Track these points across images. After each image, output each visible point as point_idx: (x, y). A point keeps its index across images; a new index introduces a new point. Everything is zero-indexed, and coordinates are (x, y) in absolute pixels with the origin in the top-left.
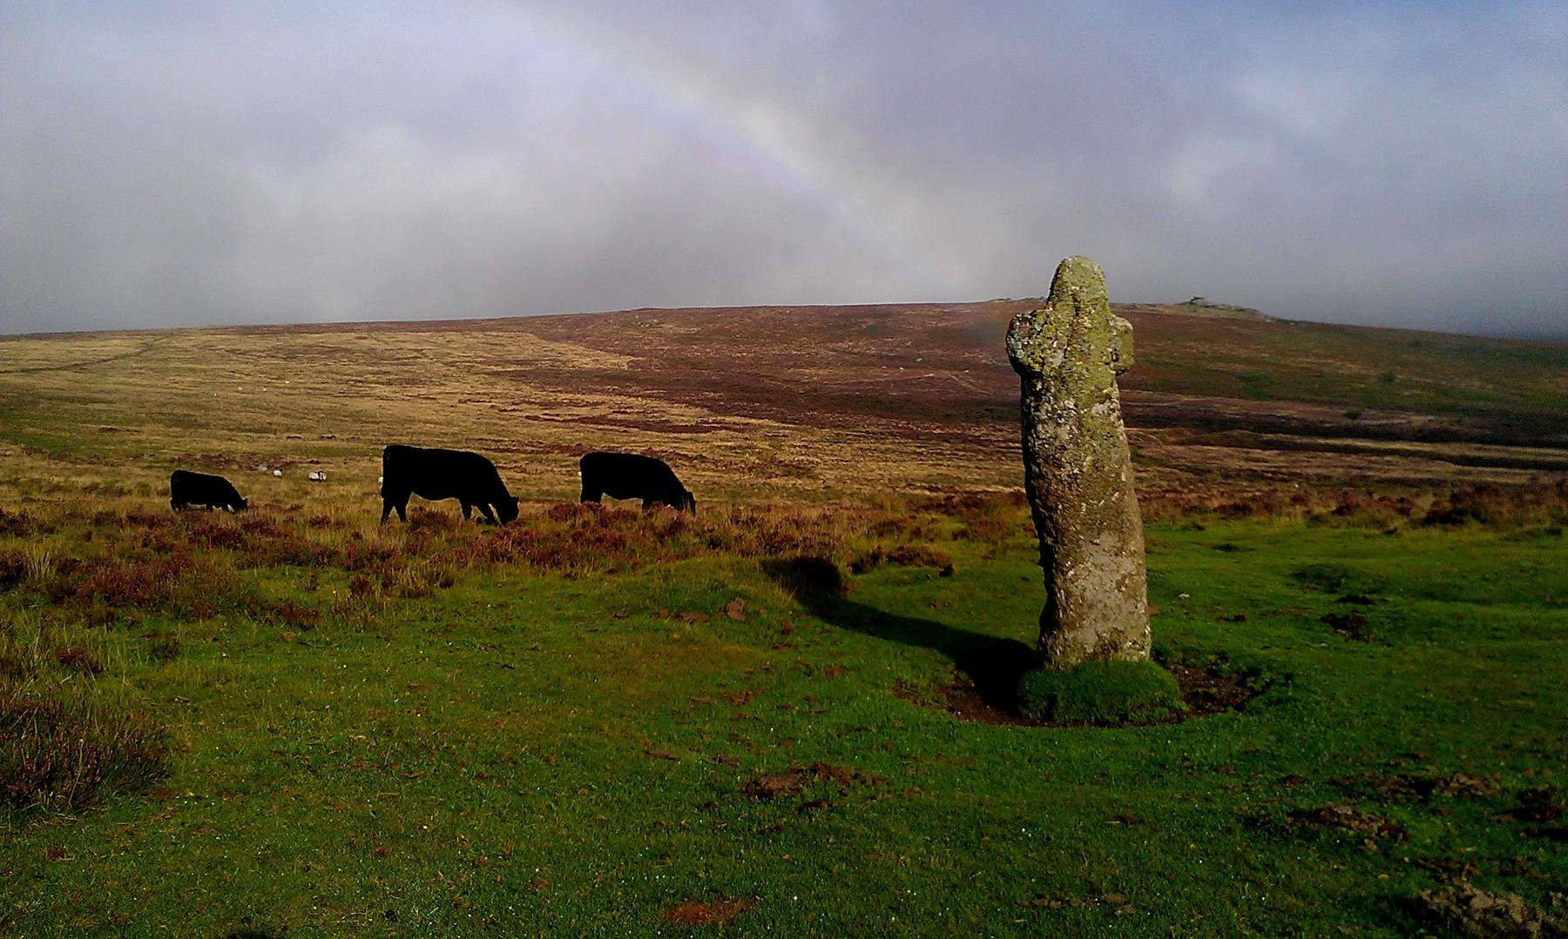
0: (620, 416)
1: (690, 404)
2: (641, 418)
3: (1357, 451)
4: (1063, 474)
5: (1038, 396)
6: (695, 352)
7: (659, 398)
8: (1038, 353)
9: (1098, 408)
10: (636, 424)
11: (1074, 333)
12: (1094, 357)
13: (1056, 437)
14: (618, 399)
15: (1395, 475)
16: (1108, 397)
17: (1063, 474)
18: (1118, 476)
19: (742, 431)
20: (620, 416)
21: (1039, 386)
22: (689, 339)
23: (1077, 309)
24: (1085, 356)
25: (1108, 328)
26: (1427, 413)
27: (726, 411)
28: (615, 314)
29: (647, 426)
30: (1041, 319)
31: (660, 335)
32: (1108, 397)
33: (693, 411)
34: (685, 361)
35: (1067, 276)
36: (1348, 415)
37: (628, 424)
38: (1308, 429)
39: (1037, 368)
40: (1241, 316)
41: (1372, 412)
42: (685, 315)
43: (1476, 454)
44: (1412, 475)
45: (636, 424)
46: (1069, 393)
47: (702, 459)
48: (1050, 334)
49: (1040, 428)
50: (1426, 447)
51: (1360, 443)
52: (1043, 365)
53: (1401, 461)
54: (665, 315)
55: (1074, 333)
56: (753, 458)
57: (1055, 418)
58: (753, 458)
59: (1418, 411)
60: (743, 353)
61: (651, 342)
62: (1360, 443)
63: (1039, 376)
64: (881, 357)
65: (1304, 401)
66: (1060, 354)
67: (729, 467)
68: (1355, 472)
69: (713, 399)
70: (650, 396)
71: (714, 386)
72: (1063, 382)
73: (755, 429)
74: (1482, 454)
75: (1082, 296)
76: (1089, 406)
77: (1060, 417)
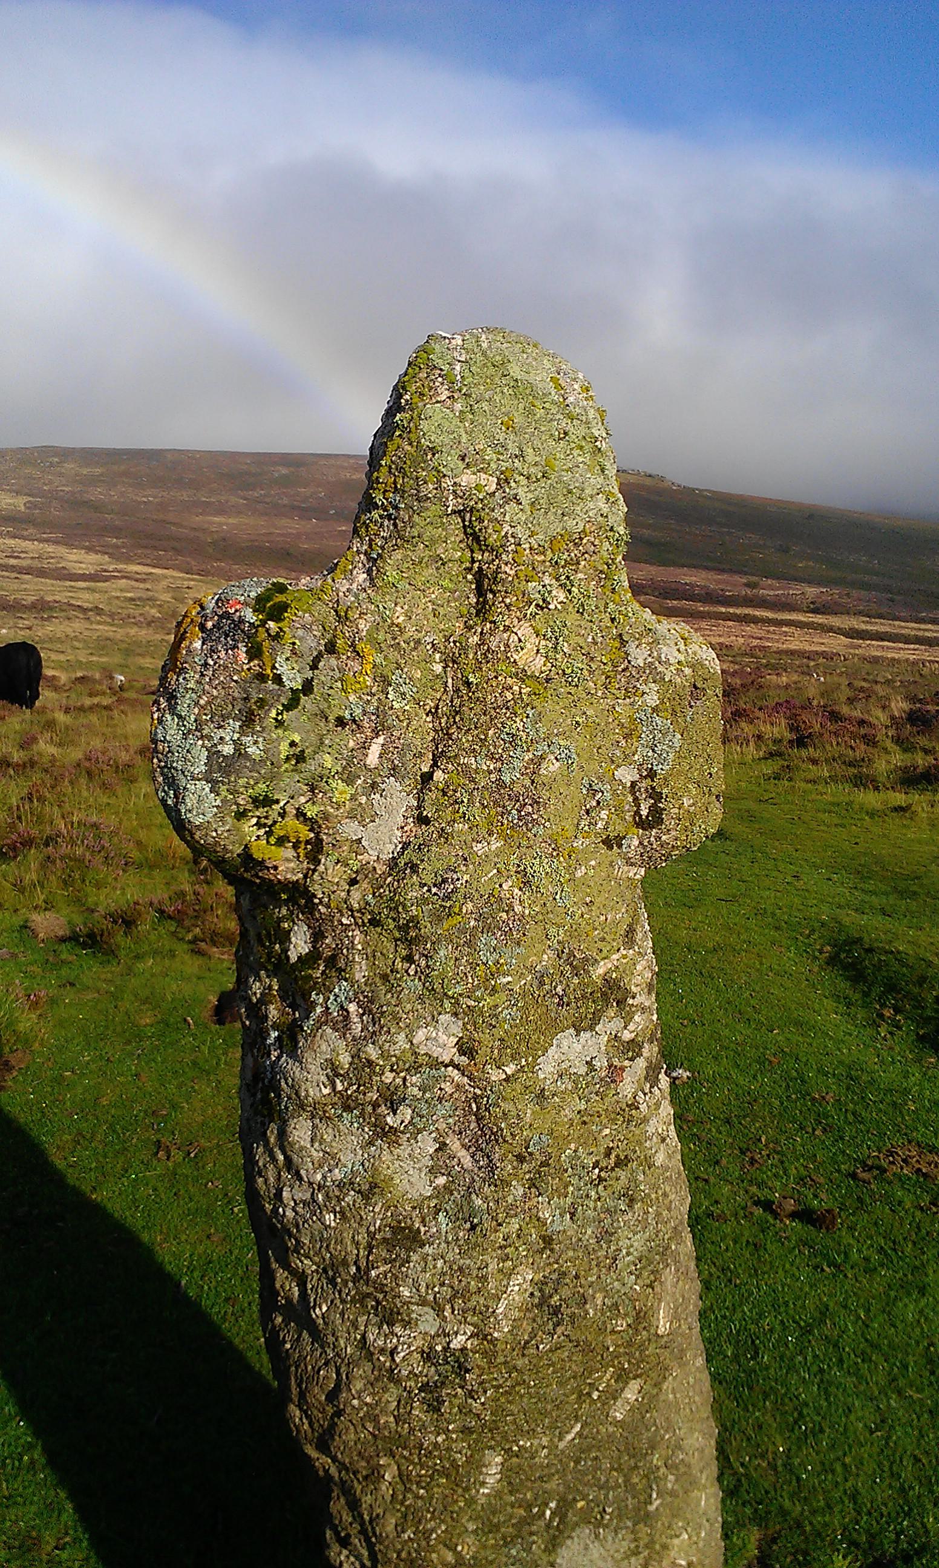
0: (12, 562)
1: (89, 549)
2: (36, 564)
3: (755, 620)
4: (407, 1345)
5: (297, 990)
6: (97, 494)
7: (56, 542)
8: (289, 791)
9: (572, 1050)
10: (28, 571)
11: (465, 706)
12: (558, 814)
13: (371, 1191)
14: (12, 542)
15: (792, 647)
16: (614, 993)
17: (407, 1345)
18: (642, 1318)
19: (144, 581)
20: (12, 562)
21: (300, 944)
22: (93, 481)
23: (484, 584)
24: (516, 808)
25: (622, 676)
26: (819, 584)
27: (128, 560)
28: (12, 450)
29: (41, 573)
30: (303, 630)
31: (61, 475)
32: (614, 993)
33: (93, 557)
34: (86, 503)
35: (437, 420)
36: (747, 585)
37: (21, 570)
38: (709, 597)
39: (286, 865)
40: (648, 482)
41: (769, 582)
42: (90, 456)
43: (863, 627)
44: (807, 648)
45: (28, 571)
46: (435, 994)
47: (98, 611)
48: (352, 704)
49: (300, 1131)
50: (819, 619)
51: (758, 613)
52: (315, 850)
53: (798, 632)
54: (66, 454)
55: (465, 706)
56: (153, 611)
57: (371, 1102)
58: (153, 611)
59: (810, 582)
60: (149, 496)
61: (51, 482)
62: (758, 613)
63: (299, 896)
64: (293, 508)
65: (706, 568)
66: (397, 800)
67: (126, 620)
68: (755, 642)
69: (117, 547)
70: (47, 541)
71: (116, 531)
72: (408, 936)
73: (157, 579)
74: (869, 627)
75: (512, 522)
76: (527, 1046)
77: (393, 1100)
